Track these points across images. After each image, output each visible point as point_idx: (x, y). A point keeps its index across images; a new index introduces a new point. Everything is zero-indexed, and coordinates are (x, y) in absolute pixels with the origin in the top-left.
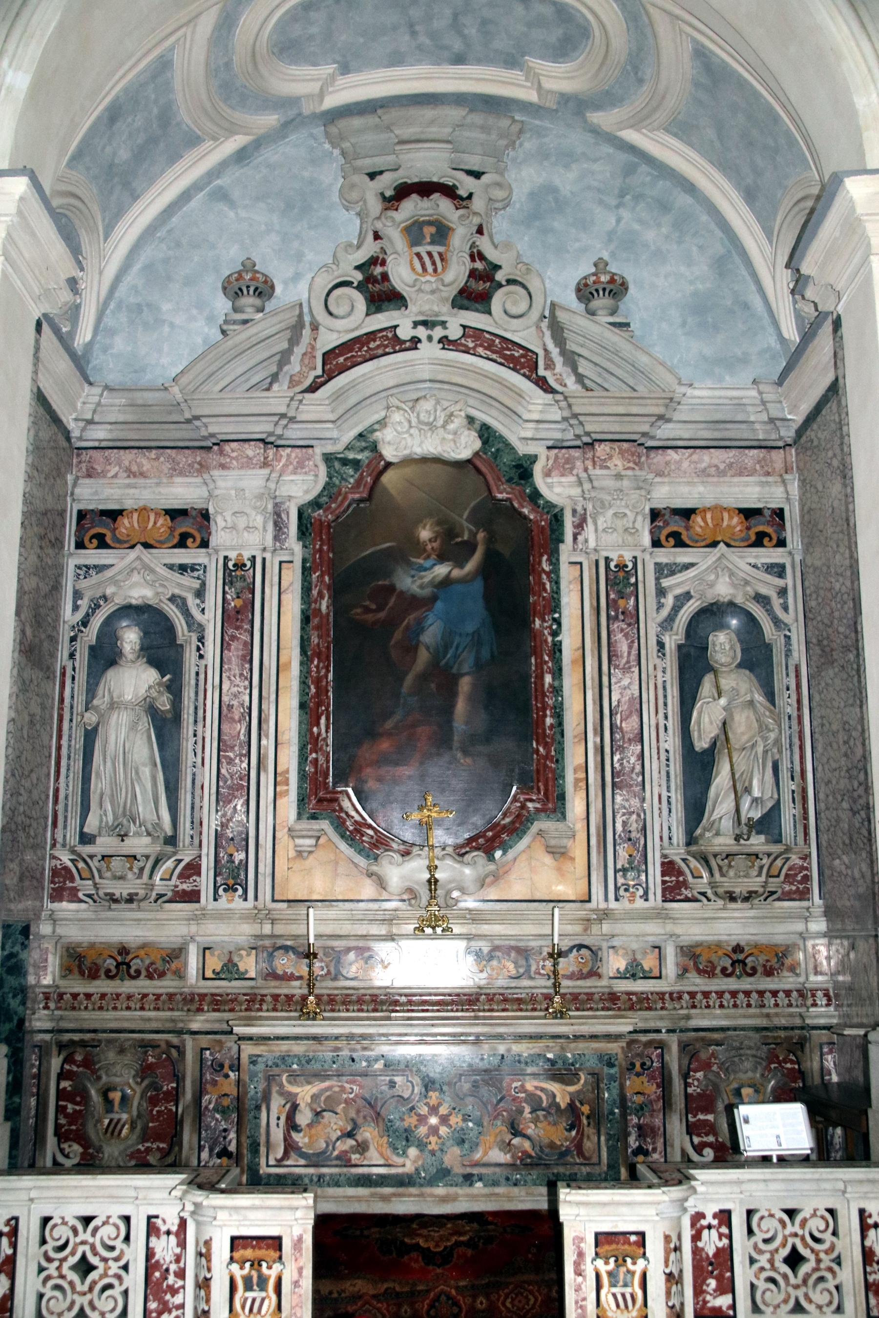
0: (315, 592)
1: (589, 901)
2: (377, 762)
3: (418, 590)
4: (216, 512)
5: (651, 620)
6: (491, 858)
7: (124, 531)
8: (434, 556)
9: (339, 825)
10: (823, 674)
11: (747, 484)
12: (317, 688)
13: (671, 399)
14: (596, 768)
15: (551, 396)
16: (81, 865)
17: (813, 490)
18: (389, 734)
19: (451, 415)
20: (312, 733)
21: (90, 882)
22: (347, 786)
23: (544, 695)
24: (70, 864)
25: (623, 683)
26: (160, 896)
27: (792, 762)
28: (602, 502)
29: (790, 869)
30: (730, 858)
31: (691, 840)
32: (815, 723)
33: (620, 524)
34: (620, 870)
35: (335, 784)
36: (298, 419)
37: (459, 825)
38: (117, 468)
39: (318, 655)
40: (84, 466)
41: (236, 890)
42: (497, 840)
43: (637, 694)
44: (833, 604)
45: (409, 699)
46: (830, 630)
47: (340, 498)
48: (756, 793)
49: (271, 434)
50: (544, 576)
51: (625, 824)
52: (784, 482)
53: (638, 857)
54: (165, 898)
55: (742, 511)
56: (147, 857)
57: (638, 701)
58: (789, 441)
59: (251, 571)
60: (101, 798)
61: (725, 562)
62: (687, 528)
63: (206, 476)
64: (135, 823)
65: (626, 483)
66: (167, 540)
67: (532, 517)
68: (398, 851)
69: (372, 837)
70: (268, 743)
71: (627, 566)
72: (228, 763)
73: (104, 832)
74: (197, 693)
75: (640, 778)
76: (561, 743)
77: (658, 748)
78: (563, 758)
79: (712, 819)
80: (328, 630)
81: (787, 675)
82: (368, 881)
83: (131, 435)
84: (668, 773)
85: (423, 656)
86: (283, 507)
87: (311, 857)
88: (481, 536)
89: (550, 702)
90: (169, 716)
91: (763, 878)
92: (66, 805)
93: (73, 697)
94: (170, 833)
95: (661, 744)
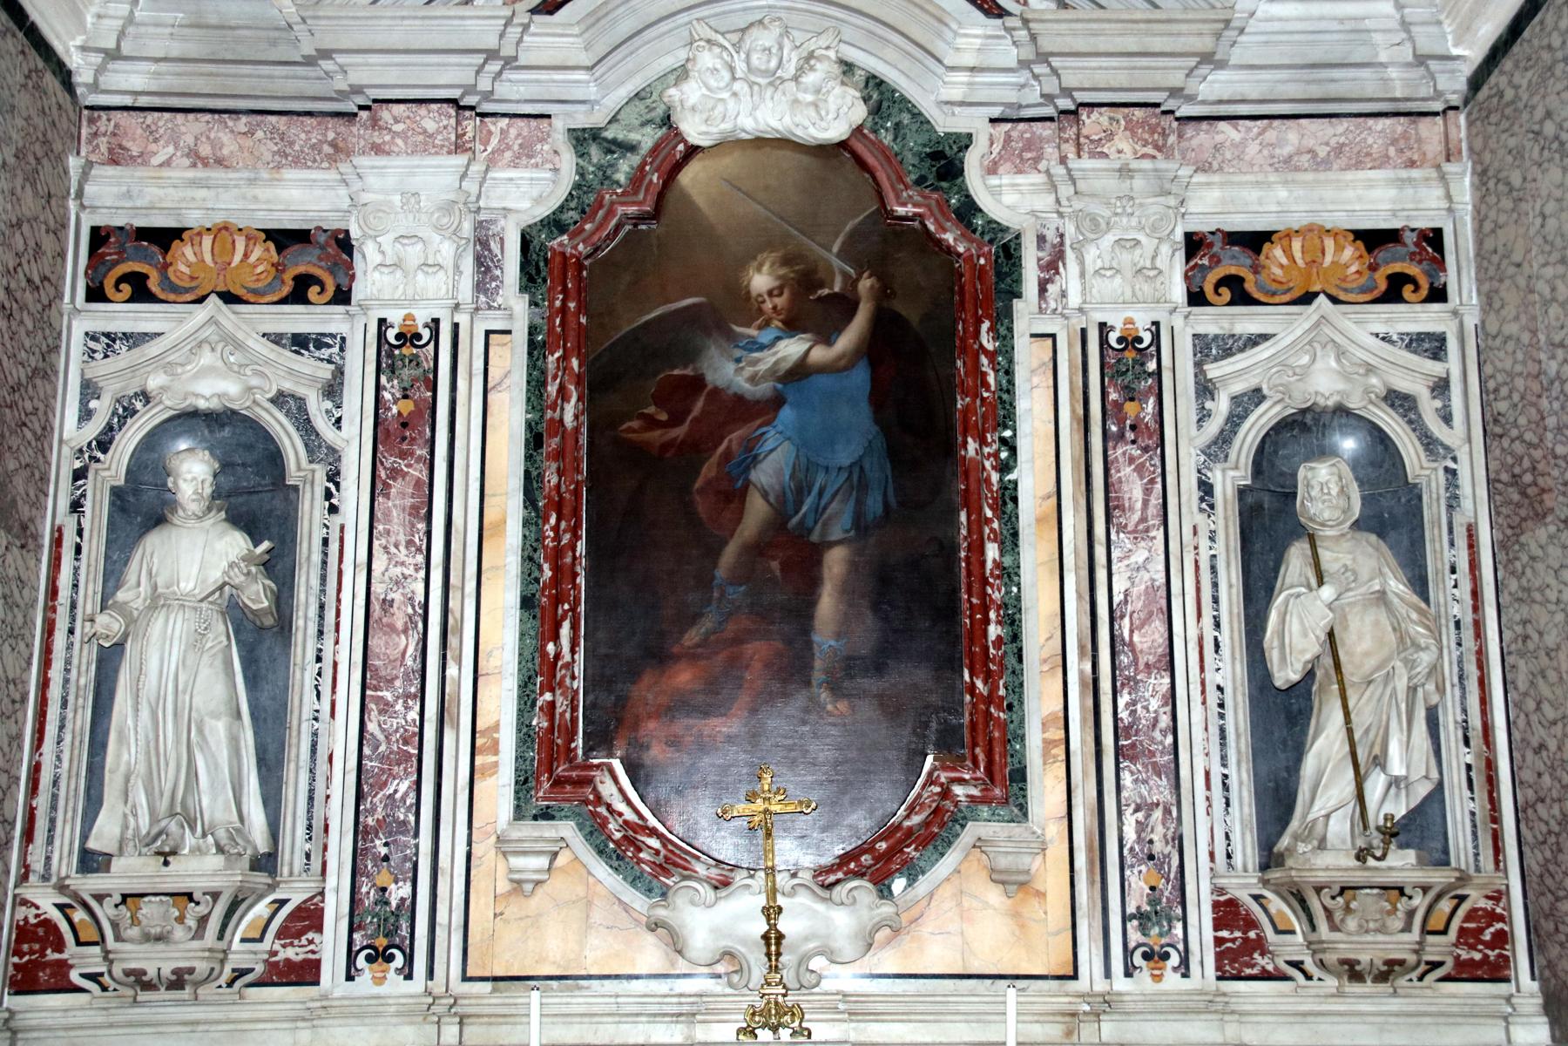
0: (552, 389)
1: (1075, 977)
2: (669, 709)
3: (747, 386)
4: (365, 235)
5: (1187, 443)
6: (885, 893)
7: (183, 268)
8: (777, 323)
9: (595, 831)
10: (1523, 539)
11: (1370, 185)
12: (556, 569)
13: (1227, 22)
14: (1083, 720)
15: (999, 22)
16: (79, 915)
17: (1501, 187)
18: (692, 657)
19: (811, 55)
20: (544, 654)
21: (97, 950)
22: (610, 756)
23: (985, 582)
24: (56, 915)
25: (1133, 559)
26: (240, 973)
27: (1464, 711)
28: (1094, 221)
29: (1469, 917)
30: (1349, 893)
31: (1270, 859)
32: (1507, 635)
33: (1126, 258)
34: (1133, 917)
35: (588, 750)
36: (522, 61)
37: (824, 829)
38: (171, 149)
39: (559, 507)
40: (103, 142)
41: (391, 958)
42: (898, 859)
43: (1161, 579)
44: (1544, 403)
45: (731, 590)
46: (1538, 454)
47: (601, 213)
48: (1397, 767)
49: (470, 89)
50: (984, 360)
51: (1141, 827)
52: (1443, 178)
53: (1168, 891)
54: (249, 978)
55: (1359, 235)
56: (216, 896)
57: (1163, 592)
58: (1455, 99)
59: (431, 347)
60: (127, 780)
61: (1327, 330)
62: (1256, 269)
63: (345, 167)
64: (193, 829)
65: (1138, 183)
66: (270, 288)
67: (961, 249)
68: (708, 880)
69: (657, 852)
70: (461, 674)
71: (1140, 340)
72: (381, 712)
73: (130, 848)
74: (323, 579)
75: (1169, 739)
76: (1017, 673)
77: (1203, 683)
78: (1021, 702)
79: (1311, 817)
80: (578, 460)
81: (1452, 544)
82: (650, 938)
83: (199, 82)
84: (1222, 730)
85: (757, 510)
86: (494, 229)
87: (540, 891)
88: (866, 284)
89: (996, 596)
90: (269, 621)
91: (1415, 935)
92: (55, 797)
93: (75, 586)
94: (262, 844)
95: (1209, 675)
